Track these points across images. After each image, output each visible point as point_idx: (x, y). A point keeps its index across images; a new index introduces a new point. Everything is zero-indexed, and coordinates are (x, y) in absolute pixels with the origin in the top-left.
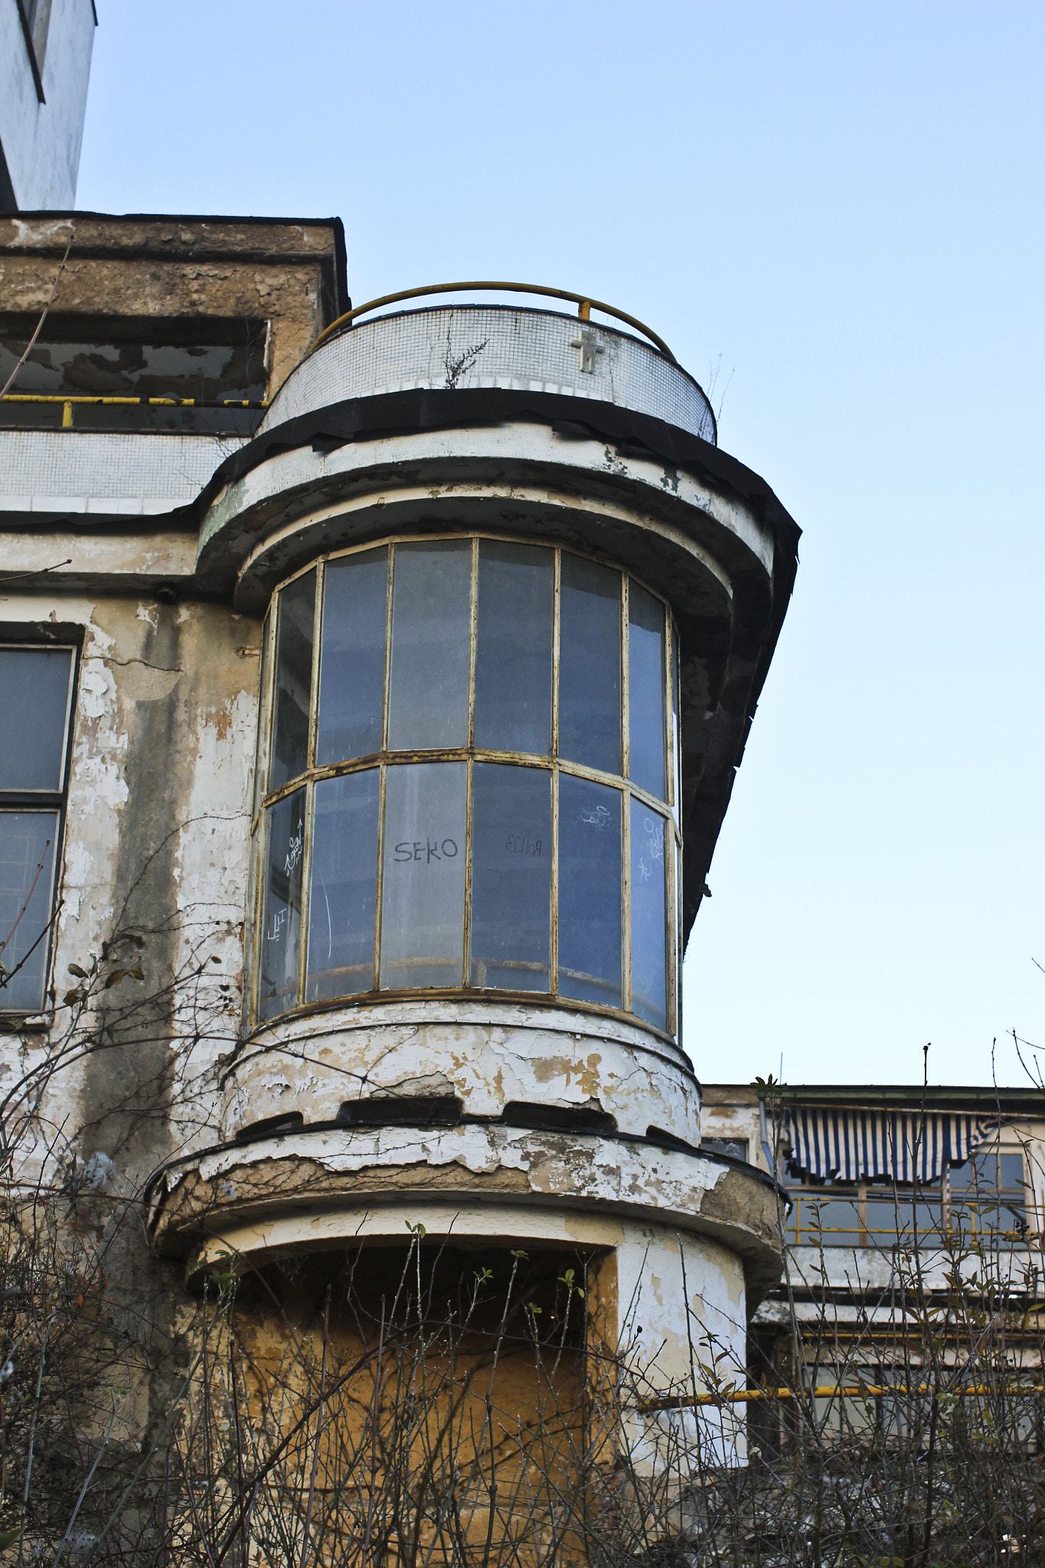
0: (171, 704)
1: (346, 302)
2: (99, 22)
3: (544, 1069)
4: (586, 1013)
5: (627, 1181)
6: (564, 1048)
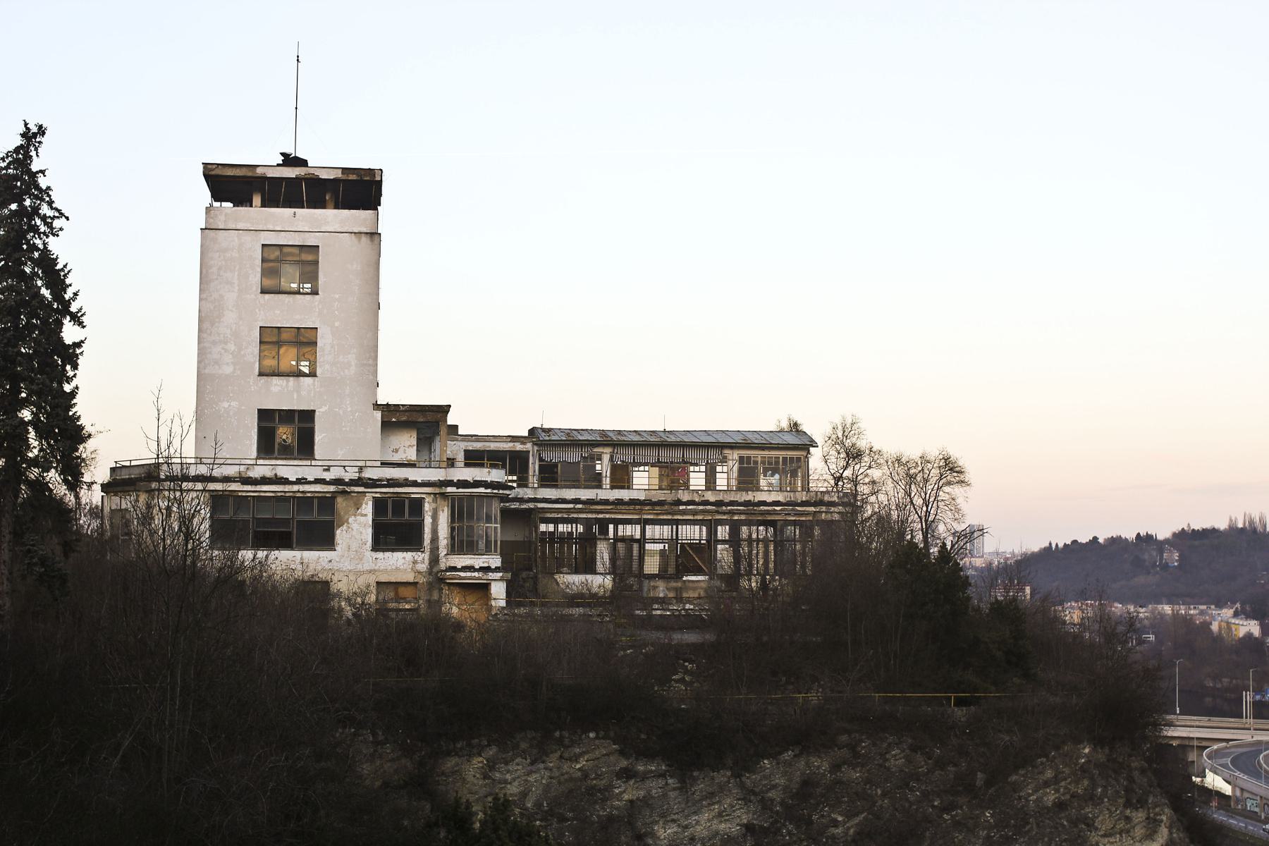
0: (437, 508)
1: (1229, 796)
2: (267, 296)
3: (483, 563)
6: (486, 560)
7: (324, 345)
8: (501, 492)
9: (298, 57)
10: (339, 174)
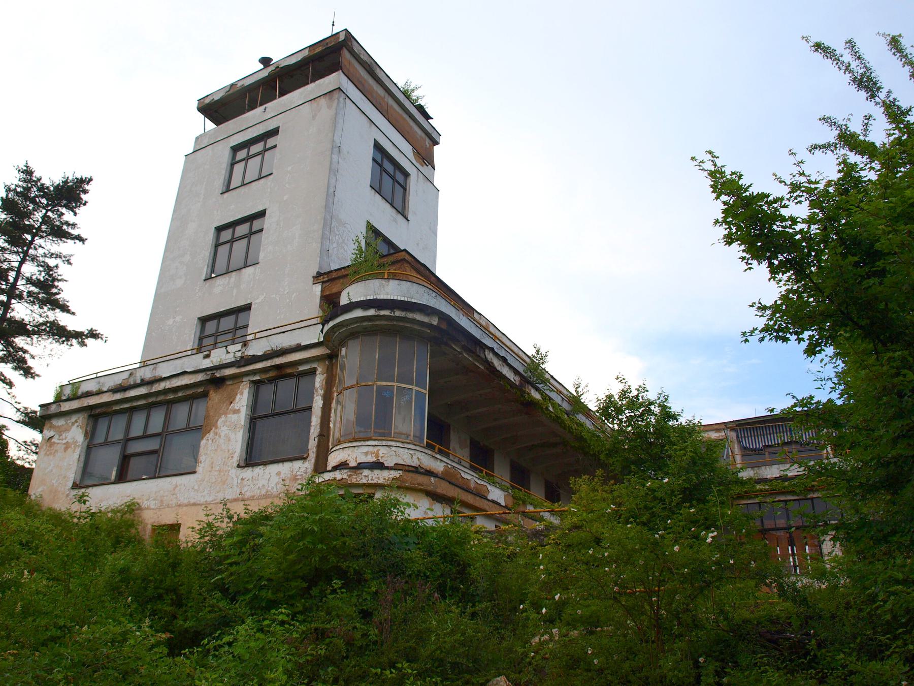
3: (366, 454)
4: (378, 440)
5: (370, 478)
6: (371, 449)
7: (271, 225)
8: (401, 324)
9: (333, 22)
10: (306, 53)
